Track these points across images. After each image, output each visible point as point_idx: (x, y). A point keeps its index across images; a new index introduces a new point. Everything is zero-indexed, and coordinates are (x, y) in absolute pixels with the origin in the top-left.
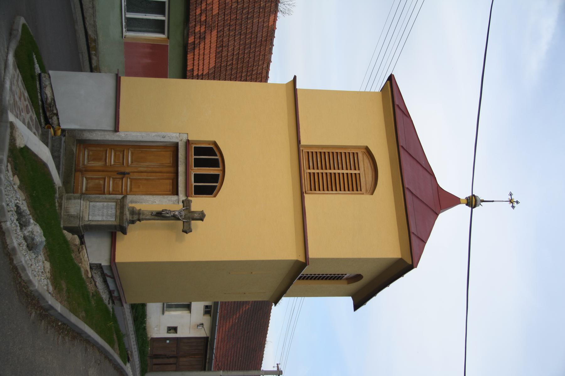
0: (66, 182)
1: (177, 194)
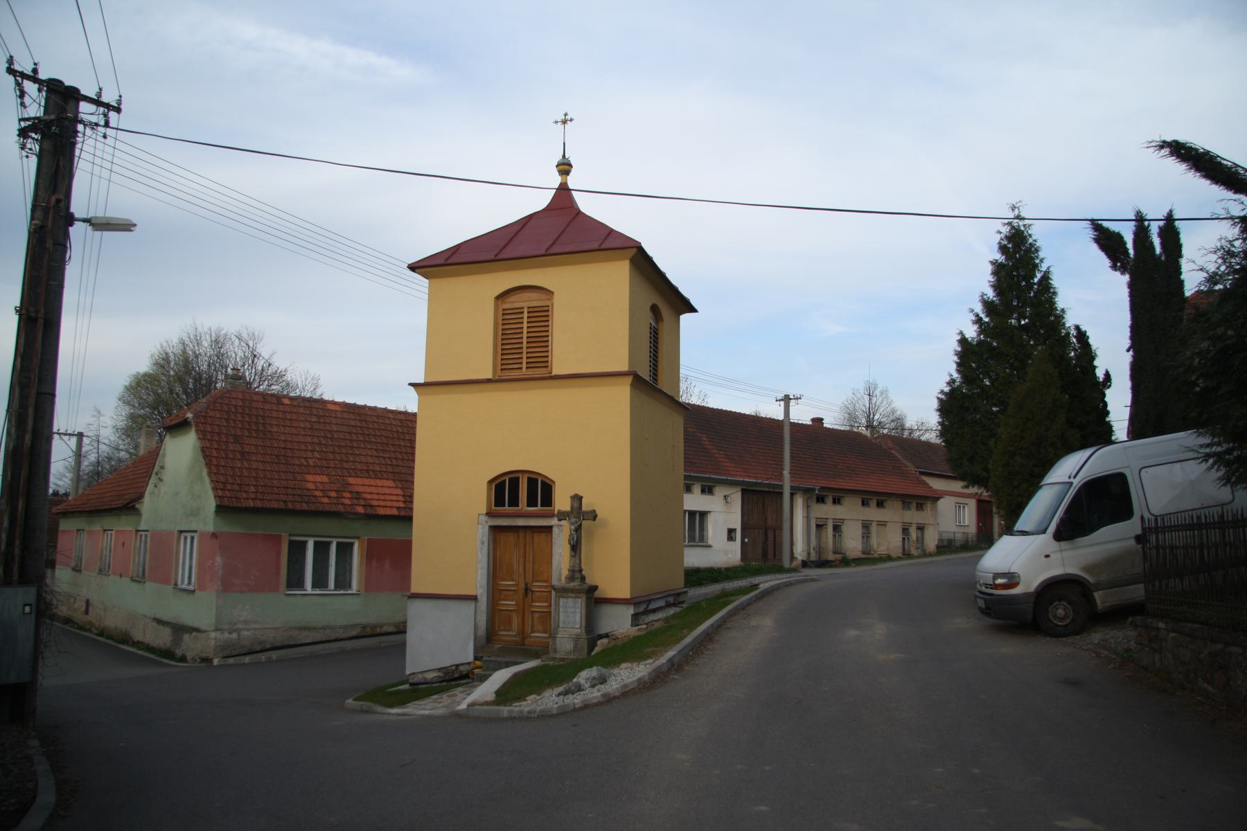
0: (536, 655)
1: (551, 527)
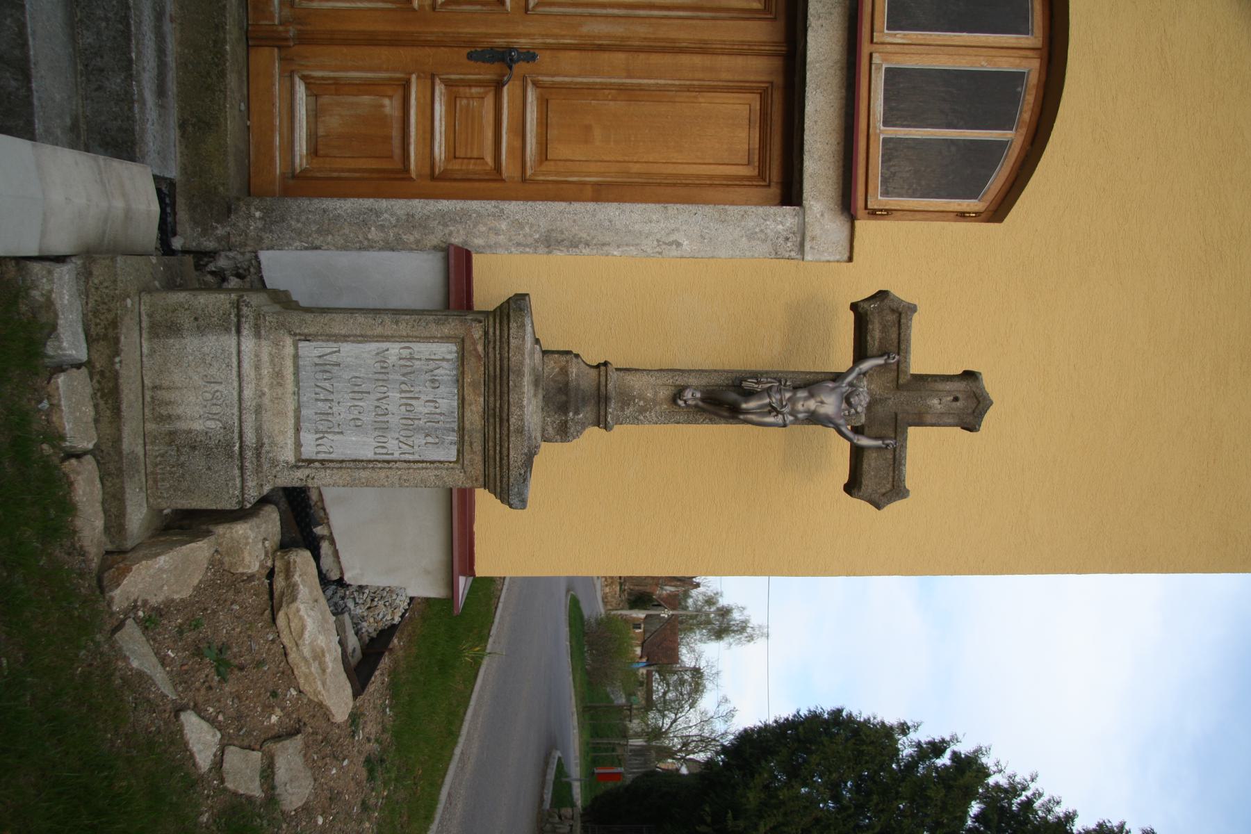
1: (791, 194)
